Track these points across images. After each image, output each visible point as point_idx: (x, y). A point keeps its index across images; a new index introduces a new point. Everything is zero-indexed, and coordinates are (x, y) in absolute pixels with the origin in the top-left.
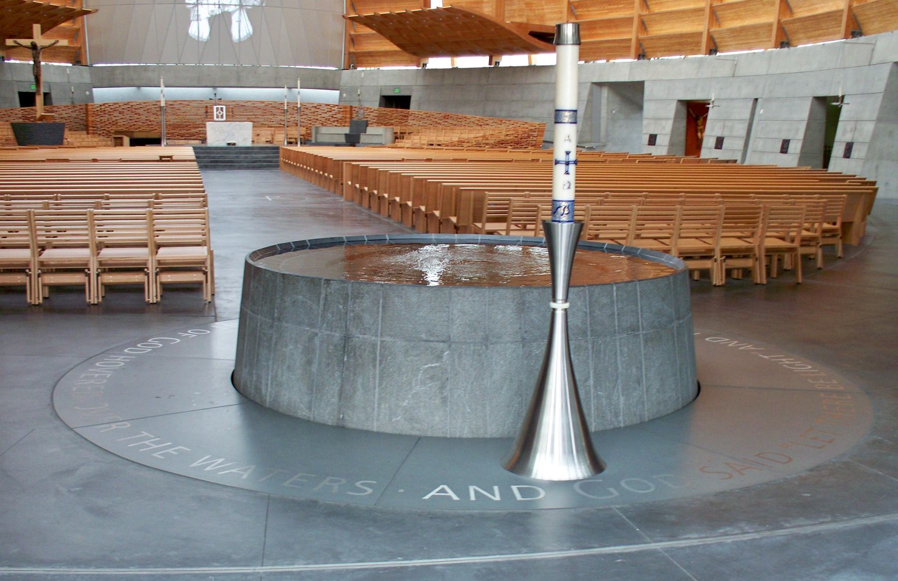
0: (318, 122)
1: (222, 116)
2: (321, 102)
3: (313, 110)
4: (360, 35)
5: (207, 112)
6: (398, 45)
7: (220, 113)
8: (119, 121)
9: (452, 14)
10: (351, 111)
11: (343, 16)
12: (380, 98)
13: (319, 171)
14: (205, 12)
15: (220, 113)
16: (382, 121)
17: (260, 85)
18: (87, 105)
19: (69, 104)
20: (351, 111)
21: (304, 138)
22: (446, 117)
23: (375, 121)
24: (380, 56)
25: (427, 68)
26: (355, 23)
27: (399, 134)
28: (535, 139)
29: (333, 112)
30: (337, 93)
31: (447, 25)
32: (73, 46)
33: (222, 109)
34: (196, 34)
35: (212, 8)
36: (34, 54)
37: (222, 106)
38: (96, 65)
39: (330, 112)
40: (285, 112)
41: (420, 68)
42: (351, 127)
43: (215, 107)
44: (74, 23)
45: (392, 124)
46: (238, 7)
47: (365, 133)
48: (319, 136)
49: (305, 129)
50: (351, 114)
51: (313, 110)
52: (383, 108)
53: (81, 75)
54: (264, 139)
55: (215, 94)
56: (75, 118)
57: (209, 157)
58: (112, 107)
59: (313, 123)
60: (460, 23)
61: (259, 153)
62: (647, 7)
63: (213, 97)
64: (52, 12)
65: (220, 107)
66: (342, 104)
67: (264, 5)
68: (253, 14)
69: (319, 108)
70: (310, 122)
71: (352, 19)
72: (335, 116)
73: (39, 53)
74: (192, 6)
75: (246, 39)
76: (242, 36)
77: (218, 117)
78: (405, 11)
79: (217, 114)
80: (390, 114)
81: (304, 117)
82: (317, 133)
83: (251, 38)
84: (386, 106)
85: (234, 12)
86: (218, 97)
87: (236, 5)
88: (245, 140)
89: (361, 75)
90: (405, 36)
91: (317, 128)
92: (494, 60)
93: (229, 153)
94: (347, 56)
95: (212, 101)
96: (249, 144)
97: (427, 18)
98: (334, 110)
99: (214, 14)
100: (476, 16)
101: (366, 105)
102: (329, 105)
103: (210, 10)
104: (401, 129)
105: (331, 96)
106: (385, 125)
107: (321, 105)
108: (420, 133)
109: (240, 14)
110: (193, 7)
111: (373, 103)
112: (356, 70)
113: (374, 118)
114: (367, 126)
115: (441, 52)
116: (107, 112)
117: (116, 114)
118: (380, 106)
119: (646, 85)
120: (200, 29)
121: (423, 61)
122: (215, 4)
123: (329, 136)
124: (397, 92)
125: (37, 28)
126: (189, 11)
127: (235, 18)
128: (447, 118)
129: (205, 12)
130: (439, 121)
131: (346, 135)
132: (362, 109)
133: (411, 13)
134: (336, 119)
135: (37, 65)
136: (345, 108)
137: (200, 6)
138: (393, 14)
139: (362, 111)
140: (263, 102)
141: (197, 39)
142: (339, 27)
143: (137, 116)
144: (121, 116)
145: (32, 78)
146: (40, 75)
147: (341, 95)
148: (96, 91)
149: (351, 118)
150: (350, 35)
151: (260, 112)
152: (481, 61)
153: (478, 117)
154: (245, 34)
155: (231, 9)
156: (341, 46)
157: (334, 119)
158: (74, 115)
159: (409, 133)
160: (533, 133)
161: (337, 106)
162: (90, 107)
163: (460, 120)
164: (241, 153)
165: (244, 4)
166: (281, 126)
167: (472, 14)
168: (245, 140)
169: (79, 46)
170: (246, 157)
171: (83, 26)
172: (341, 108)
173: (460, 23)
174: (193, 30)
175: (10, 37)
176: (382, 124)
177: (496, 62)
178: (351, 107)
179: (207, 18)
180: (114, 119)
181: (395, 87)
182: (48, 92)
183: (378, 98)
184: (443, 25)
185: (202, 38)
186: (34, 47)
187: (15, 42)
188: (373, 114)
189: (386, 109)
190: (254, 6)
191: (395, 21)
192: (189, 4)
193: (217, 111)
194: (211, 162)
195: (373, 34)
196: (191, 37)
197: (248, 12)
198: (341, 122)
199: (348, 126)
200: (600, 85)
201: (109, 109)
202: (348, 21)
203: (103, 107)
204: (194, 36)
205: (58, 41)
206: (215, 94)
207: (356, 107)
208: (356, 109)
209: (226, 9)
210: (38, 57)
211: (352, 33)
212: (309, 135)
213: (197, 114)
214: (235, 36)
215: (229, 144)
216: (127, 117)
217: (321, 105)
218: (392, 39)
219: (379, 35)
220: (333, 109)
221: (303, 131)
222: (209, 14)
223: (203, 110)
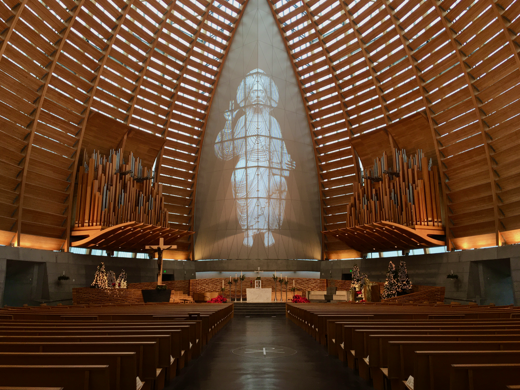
0: (309, 288)
8: (206, 289)
28: (439, 296)
33: (259, 282)
34: (247, 244)
43: (256, 281)
48: (310, 296)
62: (503, 214)
68: (274, 232)
70: (305, 288)
72: (318, 285)
76: (269, 244)
83: (274, 245)
85: (265, 232)
91: (309, 292)
92: (405, 252)
102: (315, 279)
109: (269, 234)
110: (245, 231)
112: (328, 261)
116: (199, 284)
117: (205, 285)
119: (511, 260)
120: (249, 242)
122: (256, 229)
123: (315, 296)
125: (162, 240)
127: (266, 235)
137: (249, 230)
141: (247, 246)
144: (207, 286)
148: (197, 274)
154: (271, 243)
155: (264, 231)
160: (437, 293)
177: (407, 253)
180: (203, 288)
182: (172, 273)
190: (275, 229)
193: (257, 283)
199: (325, 290)
200: (476, 263)
201: (201, 282)
209: (262, 231)
211: (326, 242)
220: (317, 281)
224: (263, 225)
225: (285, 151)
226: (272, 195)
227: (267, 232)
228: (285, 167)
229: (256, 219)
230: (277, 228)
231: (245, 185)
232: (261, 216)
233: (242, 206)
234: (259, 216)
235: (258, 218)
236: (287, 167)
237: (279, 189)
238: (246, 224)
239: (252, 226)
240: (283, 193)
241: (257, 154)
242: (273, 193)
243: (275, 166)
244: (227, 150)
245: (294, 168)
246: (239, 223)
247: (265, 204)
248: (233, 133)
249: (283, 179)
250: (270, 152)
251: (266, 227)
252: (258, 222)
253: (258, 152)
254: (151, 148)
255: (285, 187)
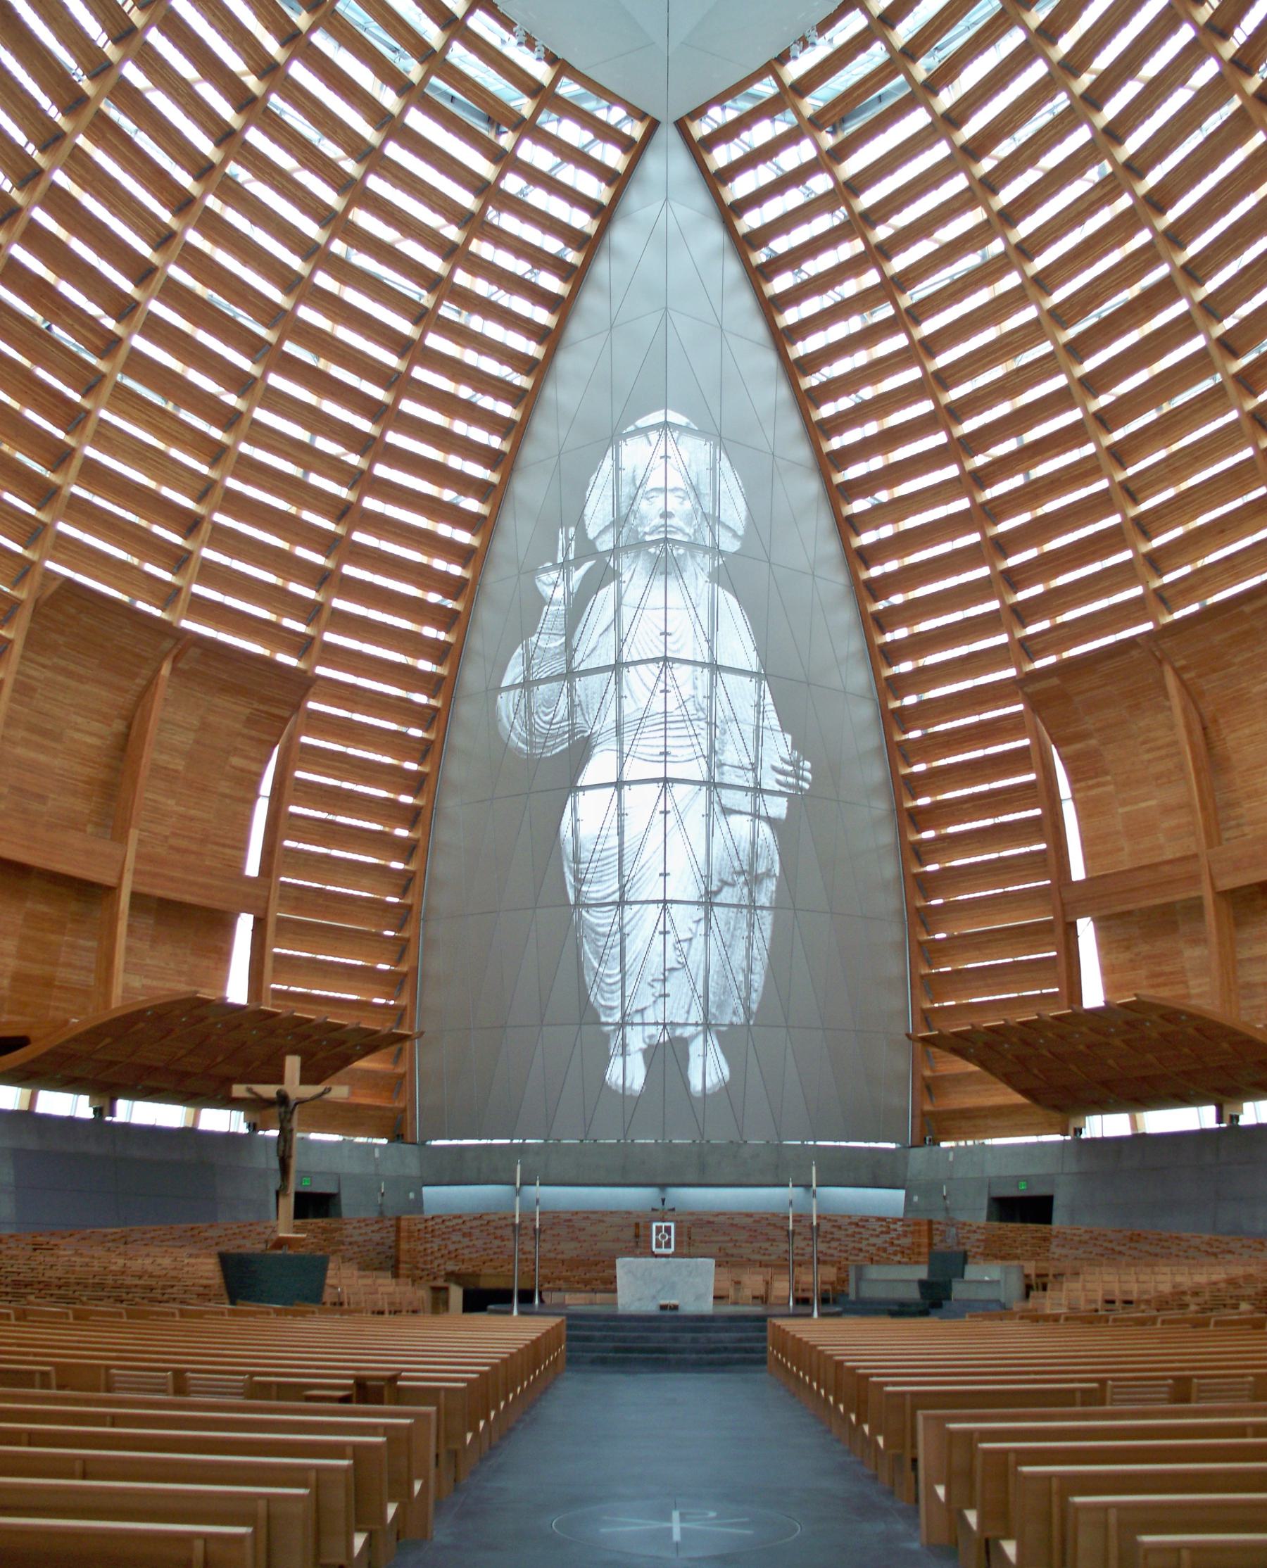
0: (862, 1255)
1: (668, 1245)
2: (868, 1213)
3: (852, 1229)
4: (943, 1077)
5: (637, 1236)
6: (1024, 1092)
7: (663, 1237)
9: (1138, 1015)
10: (930, 1230)
11: (908, 1035)
12: (990, 1206)
13: (847, 1410)
14: (637, 1039)
15: (663, 1237)
16: (995, 1251)
17: (744, 1180)
18: (398, 1219)
19: (375, 1215)
20: (930, 1230)
21: (834, 1289)
22: (1134, 1238)
23: (980, 1250)
24: (985, 1117)
25: (1083, 1136)
26: (933, 1050)
27: (1033, 1277)
29: (893, 1235)
30: (901, 1194)
31: (1126, 1042)
32: (391, 1106)
33: (668, 1230)
34: (620, 1082)
35: (651, 1030)
36: (283, 1116)
37: (667, 1224)
38: (434, 1143)
39: (888, 1233)
40: (790, 1235)
41: (1068, 1138)
42: (931, 1265)
43: (654, 1226)
44: (196, 992)
45: (1017, 1257)
46: (700, 1028)
47: (962, 1276)
48: (863, 1285)
49: (834, 1270)
50: (930, 1237)
51: (852, 1229)
52: (996, 1224)
53: (408, 1161)
54: (748, 1293)
55: (663, 1200)
56: (378, 1244)
57: (613, 1339)
58: (448, 1223)
59: (851, 1258)
60: (1154, 1035)
61: (727, 1330)
63: (658, 1205)
64: (335, 1035)
65: (663, 1225)
66: (910, 1215)
67: (751, 1022)
68: (731, 1041)
69: (864, 1227)
71: (925, 1040)
73: (292, 1113)
74: (612, 1027)
75: (717, 1089)
76: (708, 1084)
77: (659, 1245)
78: (1036, 1017)
79: (670, 1234)
80: (1012, 1235)
81: (834, 1244)
82: (859, 1278)
84: (1001, 1219)
85: (694, 1037)
86: (668, 1205)
87: (697, 1024)
88: (698, 1297)
89: (948, 1157)
90: (1036, 1071)
91: (860, 1269)
93: (658, 1330)
94: (918, 1121)
95: (655, 1213)
96: (707, 1306)
97: (1084, 1029)
98: (895, 1230)
99: (655, 1042)
100: (1191, 1016)
101: (961, 1217)
103: (646, 1034)
104: (1037, 1268)
105: (890, 1200)
106: (1003, 1258)
107: (867, 1221)
108: (1081, 1277)
109: (706, 1041)
110: (615, 1030)
111: (977, 1215)
113: (978, 1244)
114: (965, 1262)
115: (1111, 1101)
117: (456, 1237)
118: (989, 1219)
121: (1074, 1123)
122: (656, 1024)
124: (1023, 1189)
125: (293, 1064)
126: (606, 1038)
127: (696, 1048)
128: (1137, 1242)
129: (637, 1039)
130: (1118, 1248)
131: (922, 1284)
132: (953, 1226)
133: (1049, 1020)
134: (898, 1249)
135: (286, 1136)
136: (917, 1224)
137: (628, 1029)
138: (1011, 1023)
139: (953, 1230)
140: (749, 1215)
141: (621, 1091)
142: (901, 1062)
143: (497, 1242)
144: (466, 1241)
145: (275, 1164)
146: (290, 1157)
147: (908, 1198)
149: (930, 1245)
150: (924, 1078)
151: (743, 1236)
152: (1200, 1117)
153: (1206, 1237)
154: (715, 1080)
155: (688, 1032)
156: (904, 1100)
157: (895, 1248)
158: (376, 1237)
159: (1055, 1276)
161: (900, 1220)
162: (403, 1224)
163: (1166, 1244)
164: (684, 1330)
165: (713, 1022)
166: (782, 1266)
167: (1182, 1012)
168: (698, 1297)
169: (402, 1105)
170: (694, 1340)
171: (412, 1069)
172: (909, 1226)
173: (1154, 1035)
174: (614, 1074)
175: (241, 1082)
176: (996, 1257)
178: (930, 1222)
179: (641, 1049)
180: (452, 1247)
181: (1018, 1179)
183: (984, 1202)
184: (1117, 1042)
185: (631, 1087)
186: (283, 1099)
187: (250, 1090)
188: (977, 1236)
189: (1003, 1225)
191: (1015, 1040)
192: (607, 1024)
193: (657, 1234)
194: (617, 1350)
195: (971, 1074)
196: (609, 1088)
197: (720, 1036)
198: (909, 1255)
201: (442, 1226)
202: (919, 1045)
203: (430, 1223)
204: (616, 1085)
205: (330, 1090)
206: (663, 1200)
207: (939, 1223)
208: (941, 1227)
209: (678, 1032)
210: (290, 1121)
211: (927, 1073)
212: (844, 1281)
213: (618, 1240)
214: (696, 1083)
215: (663, 1307)
216: (479, 1243)
217: (867, 1221)
218: (1009, 1079)
219: (986, 1074)
220: (892, 1226)
221: (830, 1273)
222: (644, 1042)
223: (631, 1231)
224: (686, 1007)
225: (772, 719)
226: (720, 891)
227: (701, 1038)
228: (769, 782)
229: (658, 986)
230: (739, 1019)
231: (616, 850)
232: (676, 974)
233: (603, 935)
234: (667, 972)
235: (664, 981)
236: (778, 782)
237: (746, 867)
238: (617, 1003)
239: (642, 1011)
240: (762, 880)
241: (662, 733)
242: (724, 883)
243: (730, 777)
244: (546, 715)
245: (806, 786)
246: (592, 999)
247: (693, 926)
248: (569, 649)
249: (765, 830)
250: (711, 724)
251: (696, 1016)
252: (665, 996)
253: (666, 722)
254: (261, 711)
255: (771, 860)
